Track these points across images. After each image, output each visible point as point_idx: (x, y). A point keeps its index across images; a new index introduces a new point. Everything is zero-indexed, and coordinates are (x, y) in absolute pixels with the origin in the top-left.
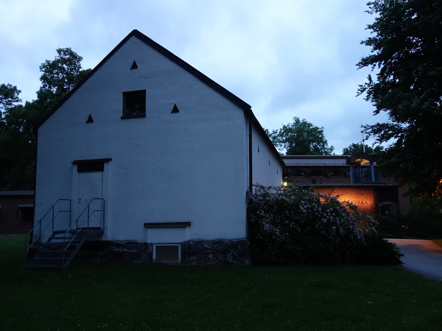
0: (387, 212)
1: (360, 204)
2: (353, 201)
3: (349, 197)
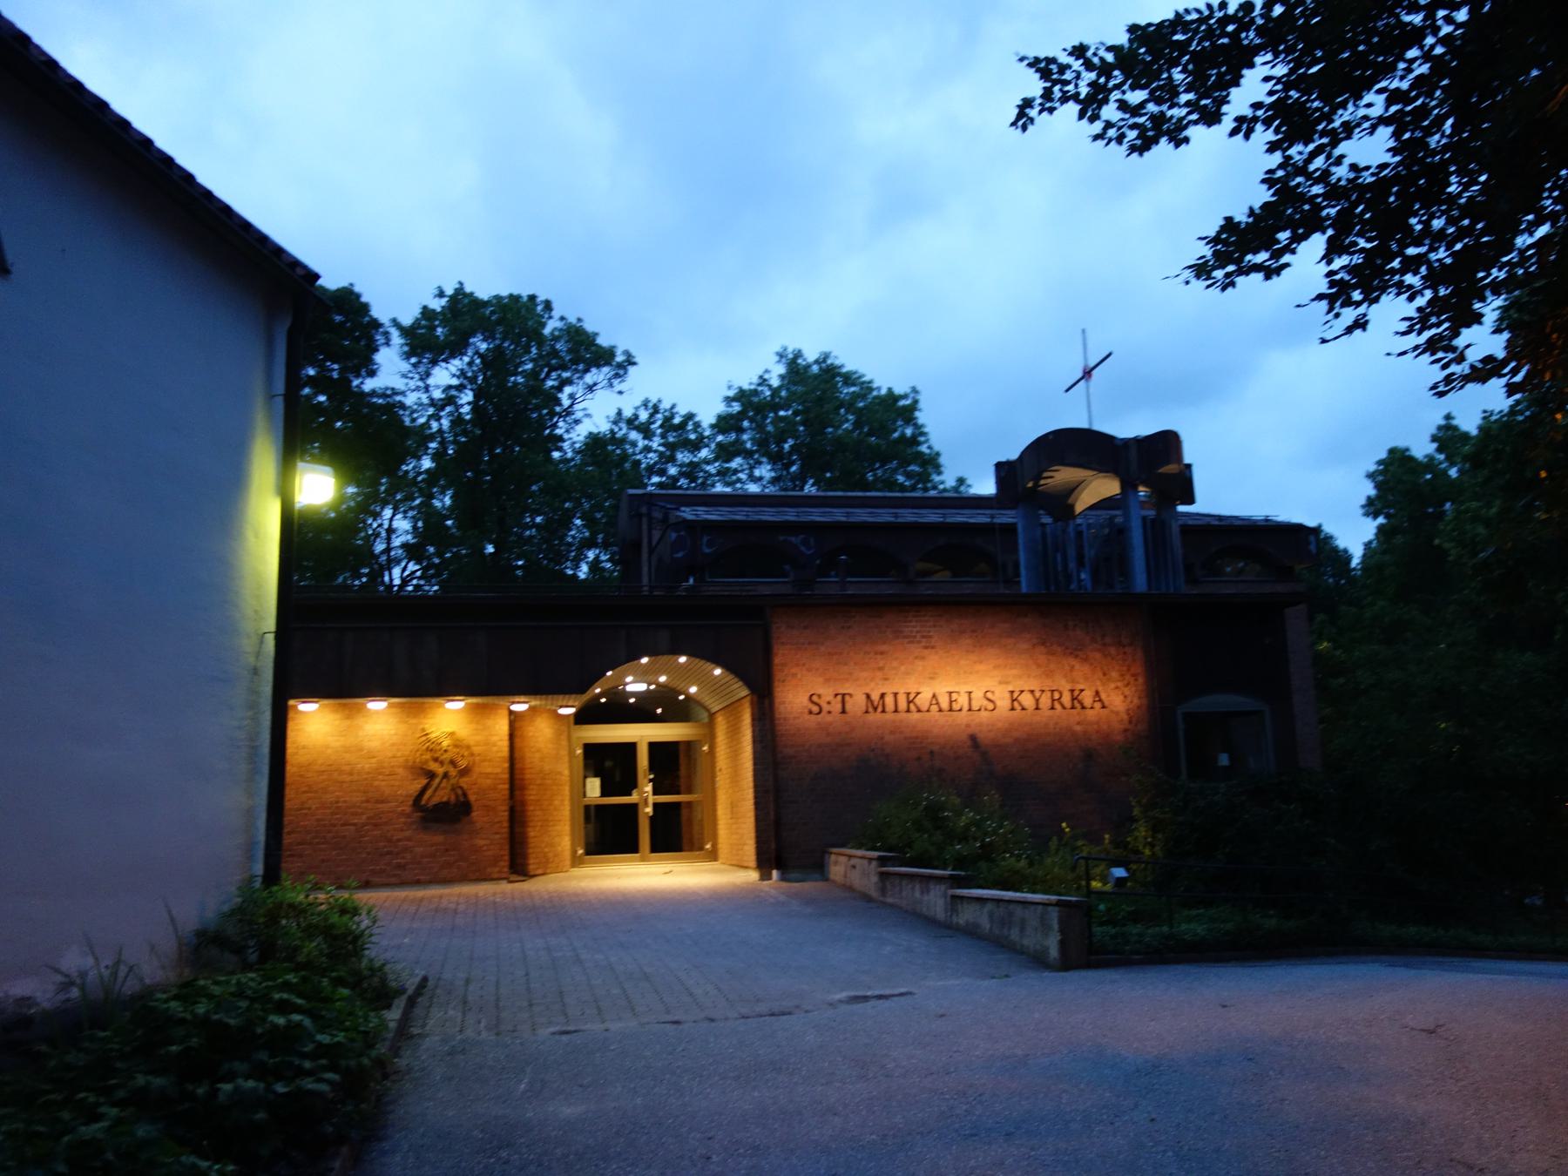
0: (1224, 760)
1: (1064, 708)
2: (1022, 691)
3: (996, 667)
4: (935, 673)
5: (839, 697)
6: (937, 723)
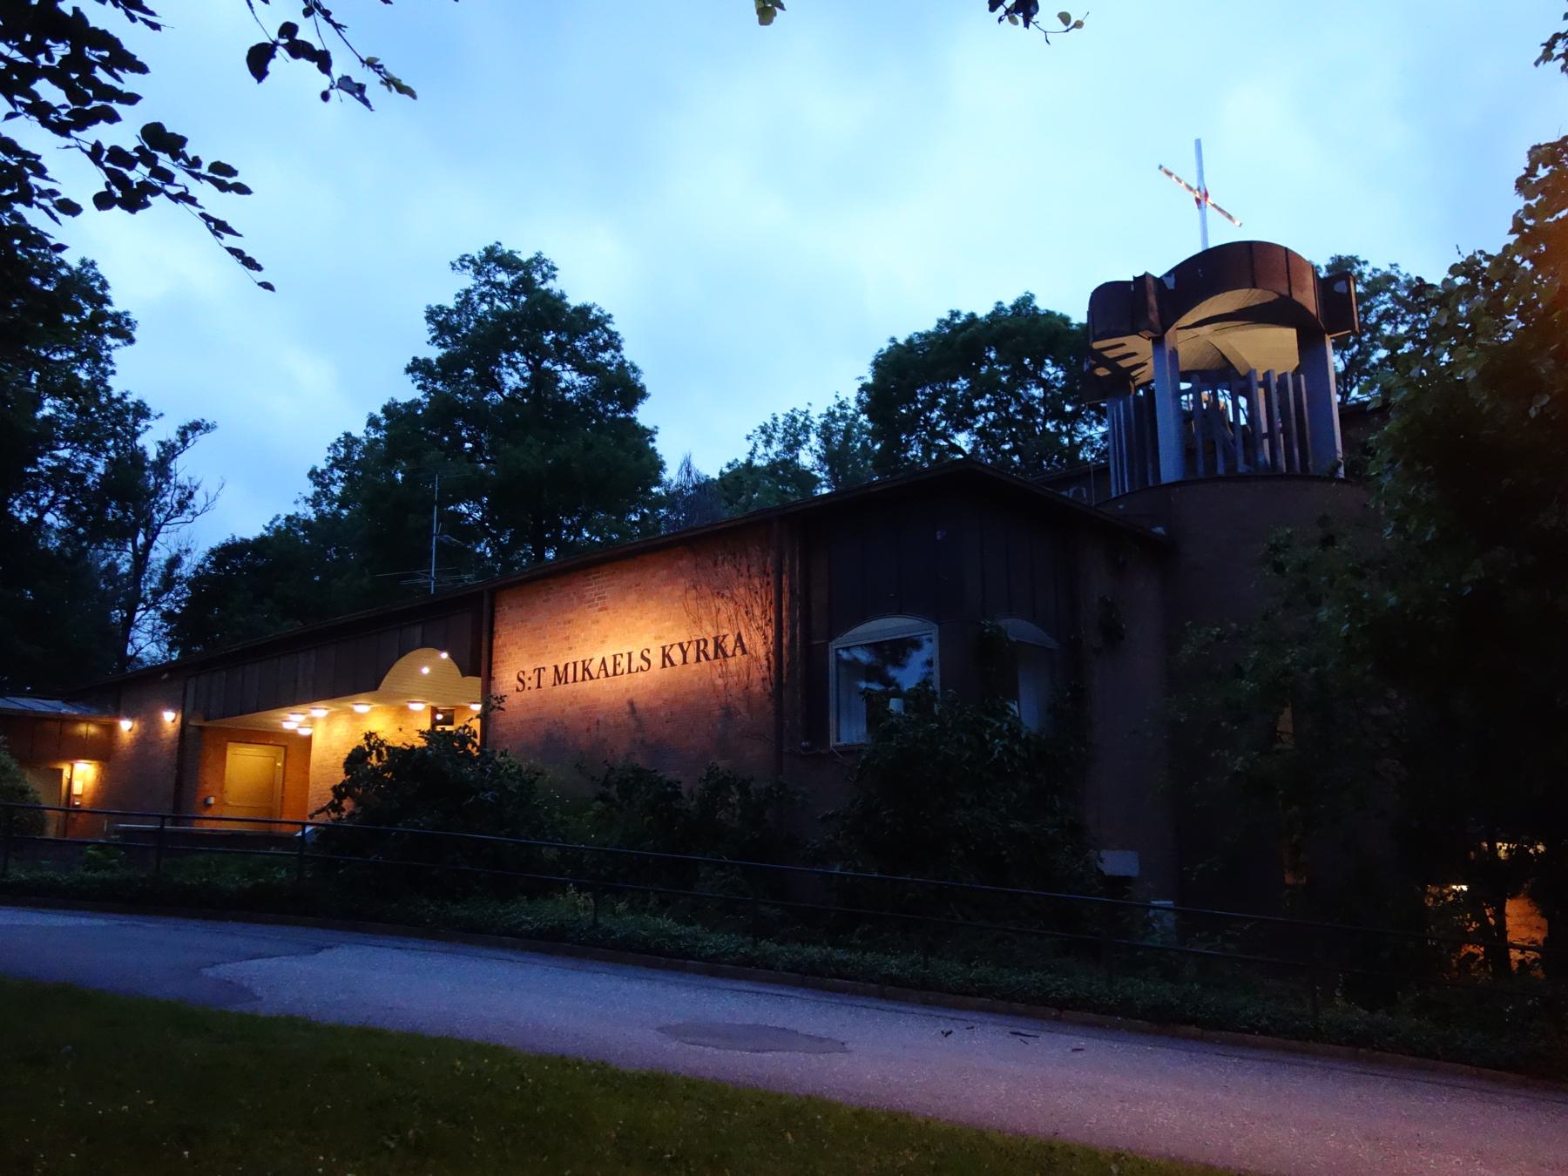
2: (672, 646)
4: (606, 636)
5: (537, 671)
6: (604, 691)
